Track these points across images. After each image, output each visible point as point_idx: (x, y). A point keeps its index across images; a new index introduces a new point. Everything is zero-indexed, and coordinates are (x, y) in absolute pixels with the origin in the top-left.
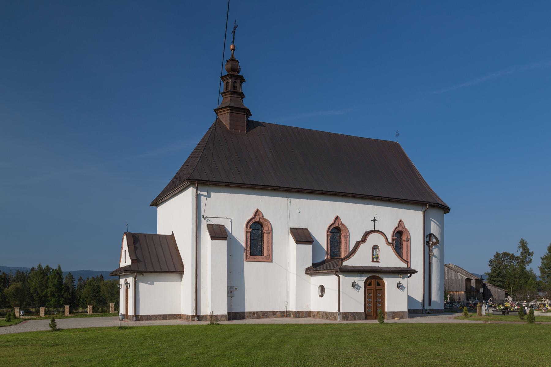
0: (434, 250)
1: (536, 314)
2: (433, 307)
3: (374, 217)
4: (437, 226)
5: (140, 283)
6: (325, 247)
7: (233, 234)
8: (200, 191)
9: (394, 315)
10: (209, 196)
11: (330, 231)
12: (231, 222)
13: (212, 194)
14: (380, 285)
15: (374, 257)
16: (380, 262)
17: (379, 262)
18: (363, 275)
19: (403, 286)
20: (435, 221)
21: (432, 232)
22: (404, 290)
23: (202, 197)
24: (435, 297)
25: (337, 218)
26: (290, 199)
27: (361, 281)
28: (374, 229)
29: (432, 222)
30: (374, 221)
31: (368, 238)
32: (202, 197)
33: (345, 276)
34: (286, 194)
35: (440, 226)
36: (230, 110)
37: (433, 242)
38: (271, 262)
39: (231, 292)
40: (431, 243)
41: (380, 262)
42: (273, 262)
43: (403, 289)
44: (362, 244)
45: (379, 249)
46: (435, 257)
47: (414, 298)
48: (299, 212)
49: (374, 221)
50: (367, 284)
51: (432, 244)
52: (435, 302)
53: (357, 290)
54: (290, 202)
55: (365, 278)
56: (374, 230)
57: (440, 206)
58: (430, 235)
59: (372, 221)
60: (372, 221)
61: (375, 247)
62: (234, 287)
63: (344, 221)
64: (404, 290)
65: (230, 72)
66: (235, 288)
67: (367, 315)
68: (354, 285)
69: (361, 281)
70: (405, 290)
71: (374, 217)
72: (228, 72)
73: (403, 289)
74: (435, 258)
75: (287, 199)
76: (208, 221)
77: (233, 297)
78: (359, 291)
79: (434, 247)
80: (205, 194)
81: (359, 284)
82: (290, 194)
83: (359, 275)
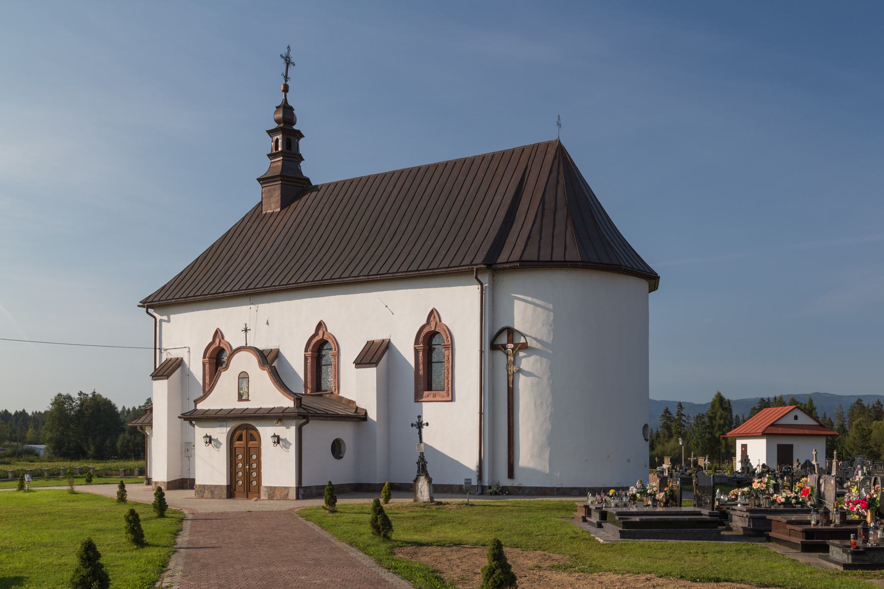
0: (523, 360)
1: (757, 504)
2: (520, 480)
3: (246, 325)
4: (540, 310)
5: (765, 440)
6: (302, 375)
7: (191, 369)
8: (161, 316)
9: (273, 492)
10: (169, 321)
11: (208, 355)
12: (189, 352)
13: (172, 316)
14: (255, 437)
15: (241, 392)
16: (250, 400)
17: (248, 400)
18: (225, 424)
19: (287, 440)
20: (529, 299)
21: (517, 326)
22: (289, 448)
23: (515, 301)
24: (526, 458)
25: (320, 325)
26: (257, 305)
27: (221, 433)
28: (246, 344)
29: (516, 302)
30: (246, 330)
31: (232, 360)
32: (515, 301)
33: (200, 427)
34: (247, 300)
35: (551, 306)
36: (281, 180)
37: (516, 345)
38: (452, 401)
39: (188, 450)
40: (511, 346)
41: (250, 400)
42: (455, 401)
43: (287, 445)
44: (223, 373)
45: (248, 378)
46: (528, 374)
47: (461, 462)
48: (267, 323)
49: (246, 330)
50: (232, 438)
51: (513, 349)
52: (525, 469)
53: (286, 450)
54: (257, 311)
55: (229, 429)
56: (245, 345)
57: (570, 265)
58: (511, 332)
59: (250, 330)
60: (250, 330)
61: (244, 377)
62: (191, 443)
63: (332, 329)
64: (289, 448)
65: (281, 123)
66: (193, 444)
67: (231, 491)
68: (209, 440)
69: (221, 433)
70: (290, 448)
71: (246, 325)
72: (279, 123)
73: (287, 445)
74: (527, 378)
75: (249, 306)
76: (168, 354)
77: (190, 458)
78: (288, 451)
79: (521, 354)
80: (165, 318)
81: (219, 439)
82: (253, 299)
83: (219, 424)
